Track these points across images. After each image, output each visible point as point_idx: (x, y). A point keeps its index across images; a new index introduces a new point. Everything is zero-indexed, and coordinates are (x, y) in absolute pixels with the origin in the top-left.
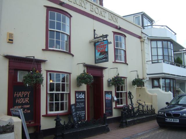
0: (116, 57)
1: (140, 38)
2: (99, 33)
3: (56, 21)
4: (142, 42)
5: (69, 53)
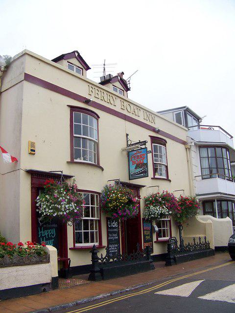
0: (155, 170)
1: (184, 143)
2: (134, 139)
3: (82, 124)
4: (188, 149)
5: (98, 166)
